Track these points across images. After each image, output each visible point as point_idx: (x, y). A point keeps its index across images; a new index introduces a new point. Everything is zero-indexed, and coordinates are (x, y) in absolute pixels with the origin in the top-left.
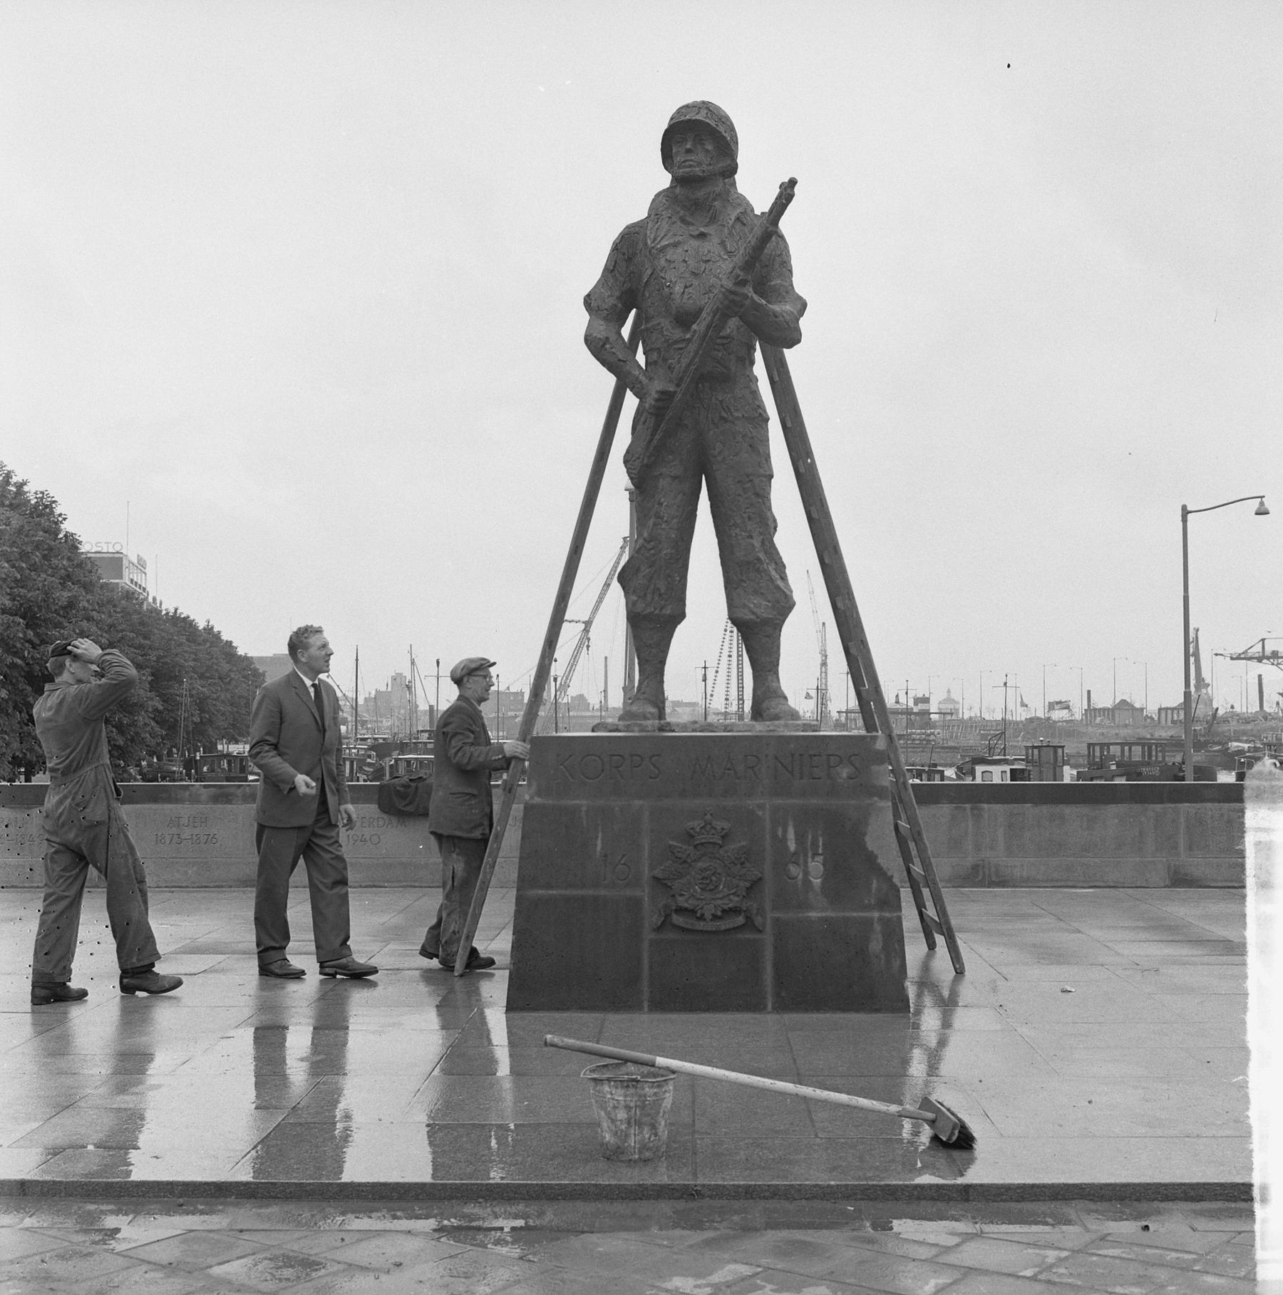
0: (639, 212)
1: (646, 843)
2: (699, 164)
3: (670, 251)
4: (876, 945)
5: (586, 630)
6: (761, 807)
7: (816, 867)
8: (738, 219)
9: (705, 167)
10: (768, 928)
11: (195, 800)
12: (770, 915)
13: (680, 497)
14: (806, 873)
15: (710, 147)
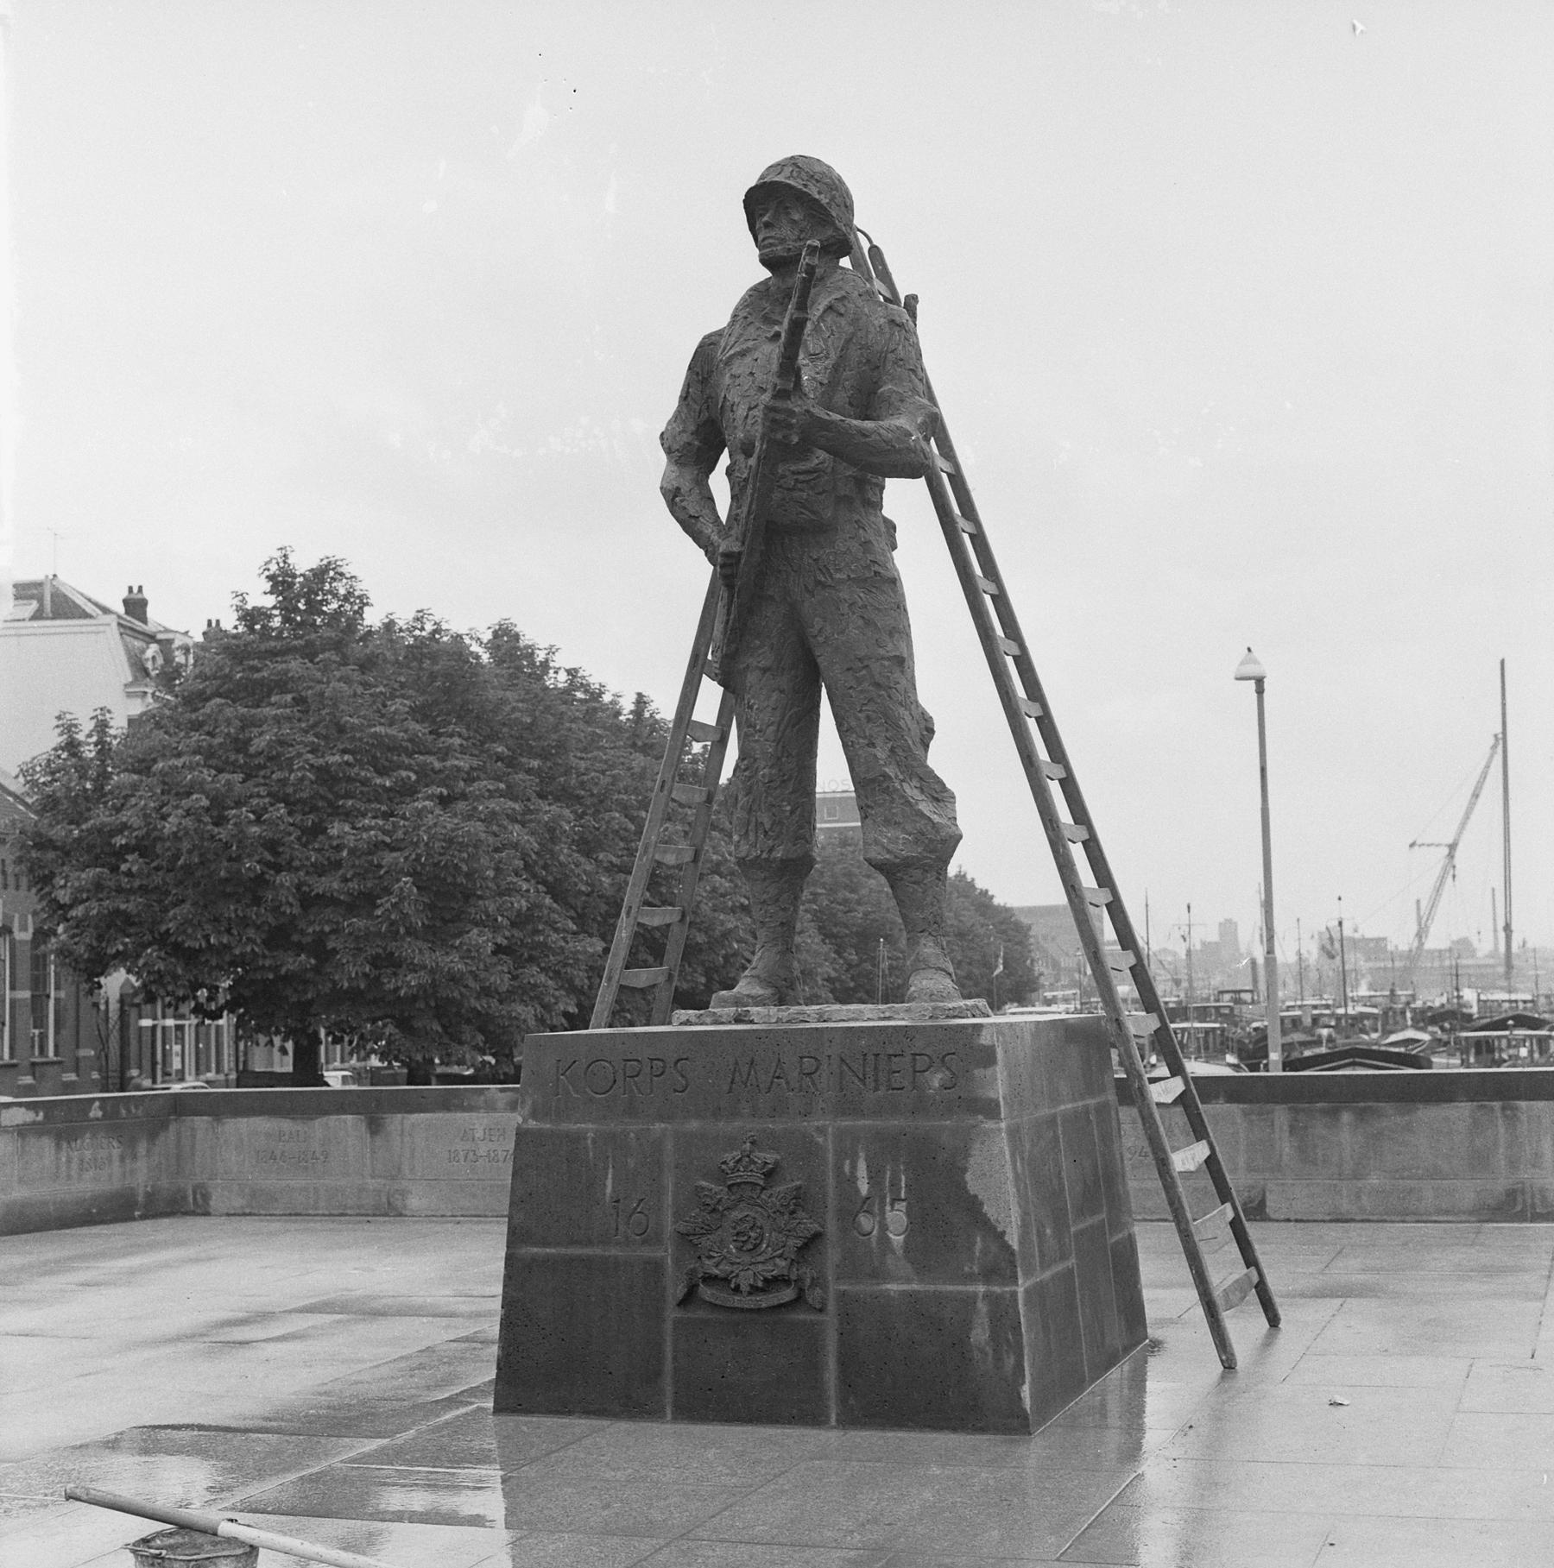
0: (719, 318)
1: (669, 1181)
2: (783, 241)
3: (737, 362)
4: (980, 1334)
5: (1451, 856)
6: (821, 1131)
7: (897, 1217)
8: (830, 308)
9: (791, 244)
10: (831, 1307)
11: (491, 1107)
12: (834, 1287)
13: (775, 696)
14: (884, 1228)
15: (796, 217)
